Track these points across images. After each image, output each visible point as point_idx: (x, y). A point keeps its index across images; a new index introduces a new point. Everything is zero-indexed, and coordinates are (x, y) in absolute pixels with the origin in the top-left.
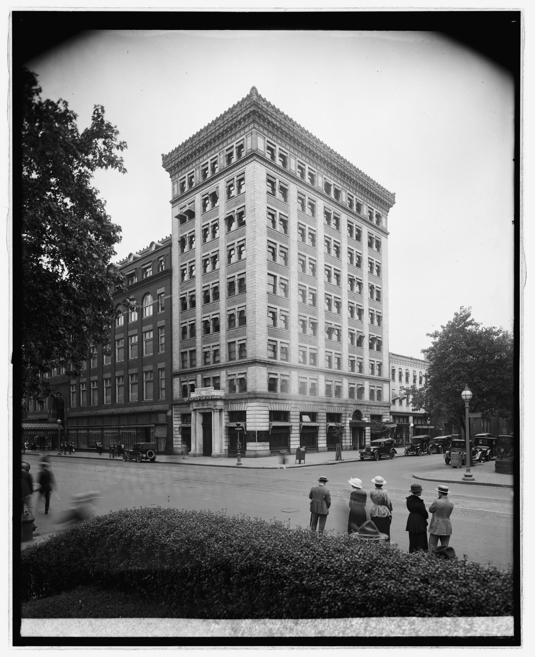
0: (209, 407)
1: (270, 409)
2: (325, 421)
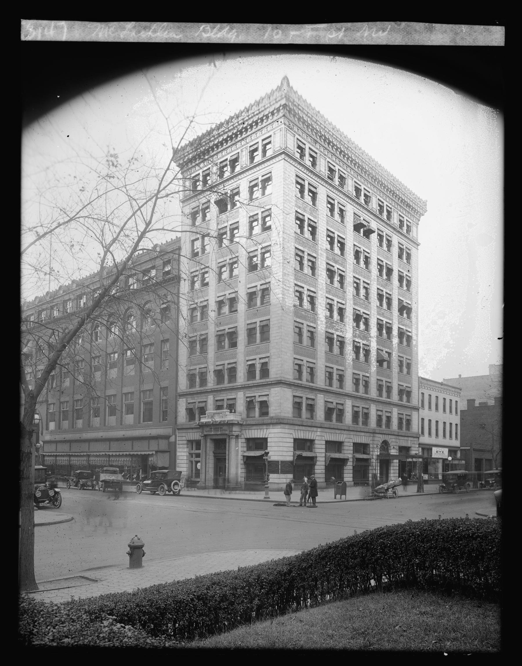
0: (224, 432)
1: (295, 437)
2: (352, 452)
